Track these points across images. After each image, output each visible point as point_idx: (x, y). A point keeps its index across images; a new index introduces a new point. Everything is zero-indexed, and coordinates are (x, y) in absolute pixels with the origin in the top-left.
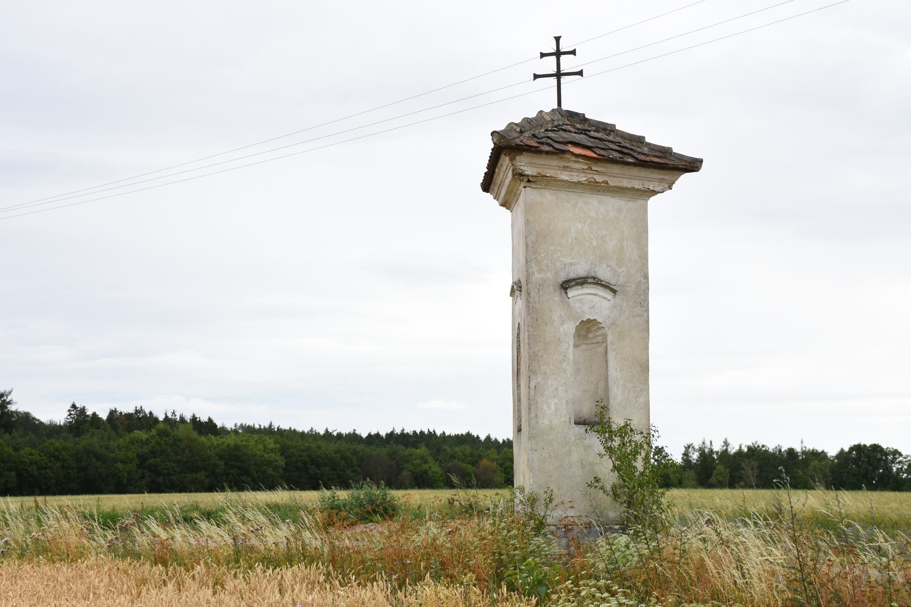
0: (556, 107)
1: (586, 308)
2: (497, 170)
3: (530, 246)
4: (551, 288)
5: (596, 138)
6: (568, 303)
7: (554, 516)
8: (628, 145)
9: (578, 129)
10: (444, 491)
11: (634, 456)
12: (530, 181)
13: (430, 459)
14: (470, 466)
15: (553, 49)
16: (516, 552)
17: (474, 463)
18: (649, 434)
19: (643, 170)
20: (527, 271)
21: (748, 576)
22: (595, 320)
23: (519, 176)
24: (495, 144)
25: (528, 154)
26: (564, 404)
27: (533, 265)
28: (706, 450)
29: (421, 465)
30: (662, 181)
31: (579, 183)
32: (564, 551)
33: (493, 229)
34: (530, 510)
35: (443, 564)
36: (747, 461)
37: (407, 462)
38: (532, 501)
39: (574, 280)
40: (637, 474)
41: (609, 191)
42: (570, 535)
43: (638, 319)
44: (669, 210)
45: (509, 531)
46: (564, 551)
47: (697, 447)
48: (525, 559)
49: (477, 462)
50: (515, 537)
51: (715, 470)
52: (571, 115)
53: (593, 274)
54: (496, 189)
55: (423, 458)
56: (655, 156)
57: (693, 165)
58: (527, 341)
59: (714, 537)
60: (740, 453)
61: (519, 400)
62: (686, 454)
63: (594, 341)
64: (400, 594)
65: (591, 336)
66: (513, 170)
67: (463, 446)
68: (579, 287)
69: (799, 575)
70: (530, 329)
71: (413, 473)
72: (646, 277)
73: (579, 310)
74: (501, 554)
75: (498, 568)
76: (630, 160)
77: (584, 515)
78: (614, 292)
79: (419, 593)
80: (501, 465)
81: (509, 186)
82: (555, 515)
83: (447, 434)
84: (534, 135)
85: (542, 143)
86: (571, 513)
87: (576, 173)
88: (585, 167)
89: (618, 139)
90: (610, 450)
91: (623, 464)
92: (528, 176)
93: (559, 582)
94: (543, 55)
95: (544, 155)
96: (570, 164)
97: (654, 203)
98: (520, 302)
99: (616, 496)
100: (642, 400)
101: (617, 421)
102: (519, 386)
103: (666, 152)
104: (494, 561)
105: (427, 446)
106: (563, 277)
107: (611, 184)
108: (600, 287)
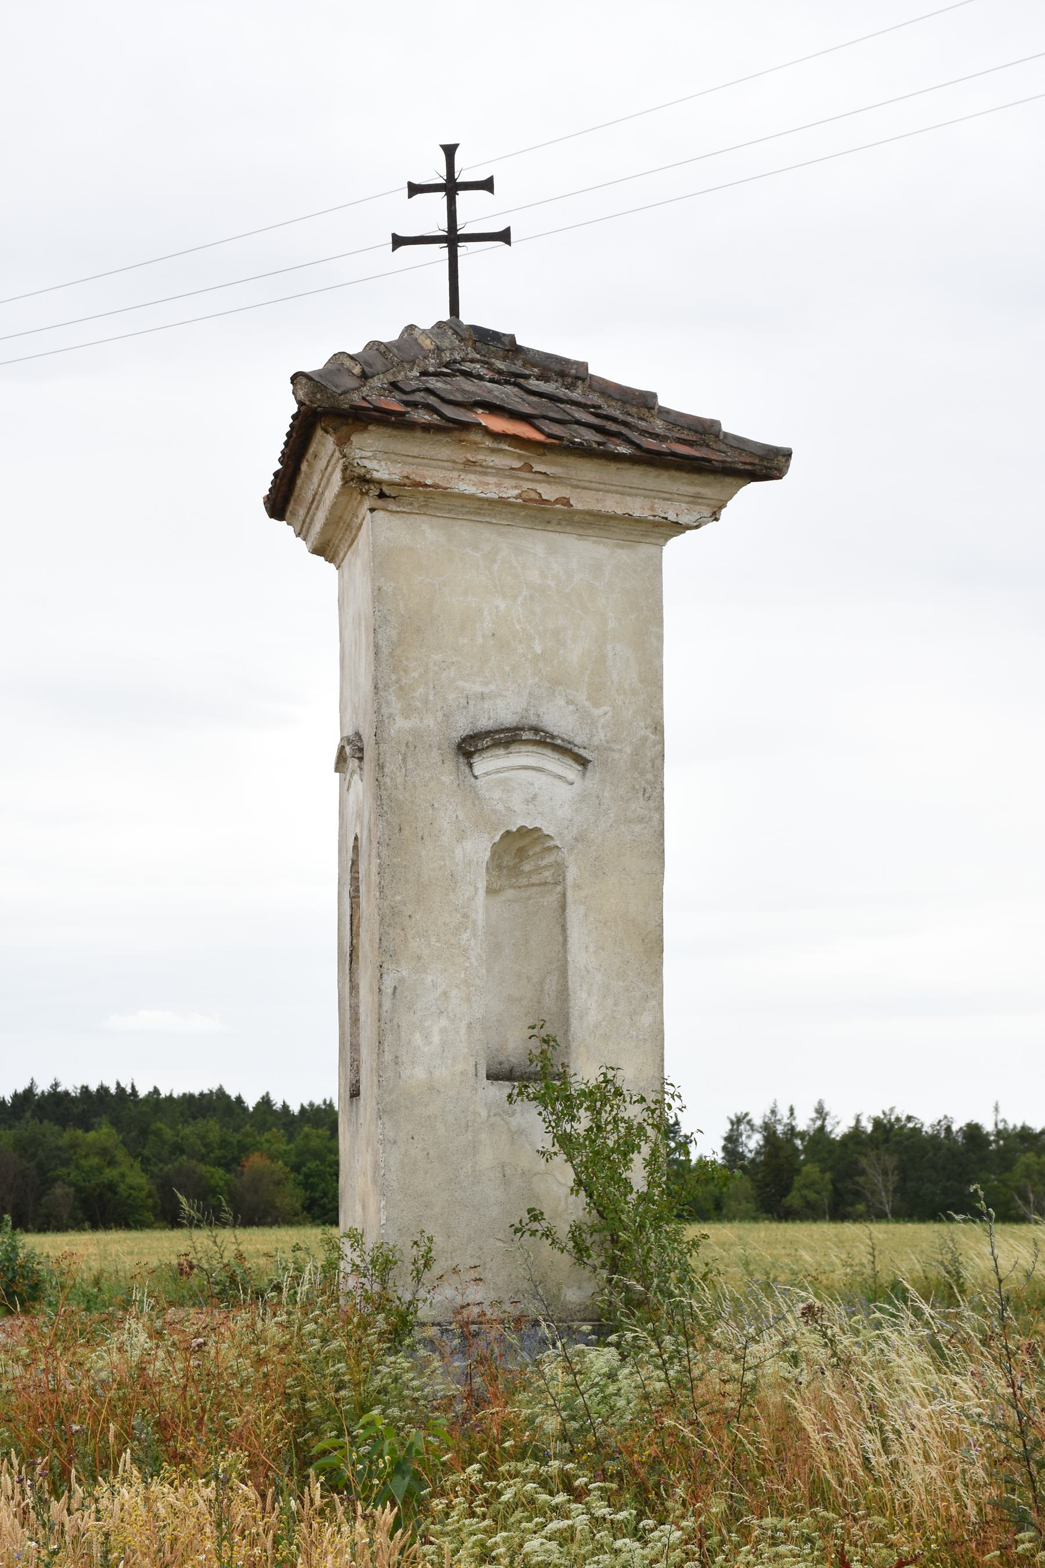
0: (446, 316)
1: (517, 802)
2: (304, 467)
3: (385, 651)
4: (435, 754)
5: (540, 395)
6: (473, 789)
7: (434, 1303)
8: (617, 414)
9: (500, 372)
10: (157, 1234)
11: (625, 1155)
12: (384, 494)
13: (120, 1154)
14: (221, 1172)
15: (437, 174)
16: (343, 1393)
17: (229, 1164)
18: (660, 1102)
19: (652, 473)
20: (378, 712)
21: (896, 1447)
22: (537, 830)
23: (359, 482)
24: (300, 403)
25: (381, 430)
26: (463, 1030)
27: (393, 698)
28: (780, 1129)
29: (100, 1170)
30: (695, 499)
31: (502, 502)
32: (456, 1389)
33: (296, 603)
34: (377, 1288)
35: (161, 1425)
36: (872, 1154)
37: (66, 1163)
38: (384, 1264)
39: (488, 733)
40: (632, 1197)
41: (571, 522)
42: (480, 1347)
43: (637, 828)
44: (713, 567)
45: (324, 1341)
46: (456, 1389)
47: (758, 1122)
48: (364, 1409)
49: (236, 1160)
50: (340, 1355)
51: (801, 1174)
52: (483, 337)
53: (533, 721)
54: (302, 512)
55: (103, 1152)
56: (679, 441)
57: (767, 464)
58: (375, 878)
59: (821, 1355)
60: (855, 1135)
61: (355, 1020)
62: (732, 1140)
63: (535, 879)
64: (56, 1507)
65: (527, 867)
66: (345, 469)
67: (201, 1123)
68: (501, 751)
69: (1016, 1445)
70: (385, 852)
71: (79, 1190)
72: (658, 728)
73: (500, 807)
74: (304, 1399)
75: (298, 1433)
76: (623, 449)
77: (506, 1297)
78: (583, 762)
79: (104, 1503)
80: (296, 1168)
81: (334, 505)
82: (438, 1298)
83: (164, 1093)
84: (394, 385)
85: (414, 405)
86: (475, 1294)
87: (494, 477)
88: (517, 464)
89: (594, 399)
90: (565, 1141)
91: (597, 1168)
92: (380, 482)
93: (448, 1468)
94: (414, 189)
95: (419, 434)
96: (480, 457)
97: (676, 551)
98: (359, 786)
99: (581, 1251)
100: (646, 1019)
101: (585, 1073)
102: (354, 988)
103: (705, 431)
104: (289, 1415)
105: (116, 1123)
106: (462, 727)
107: (577, 505)
108: (548, 752)
